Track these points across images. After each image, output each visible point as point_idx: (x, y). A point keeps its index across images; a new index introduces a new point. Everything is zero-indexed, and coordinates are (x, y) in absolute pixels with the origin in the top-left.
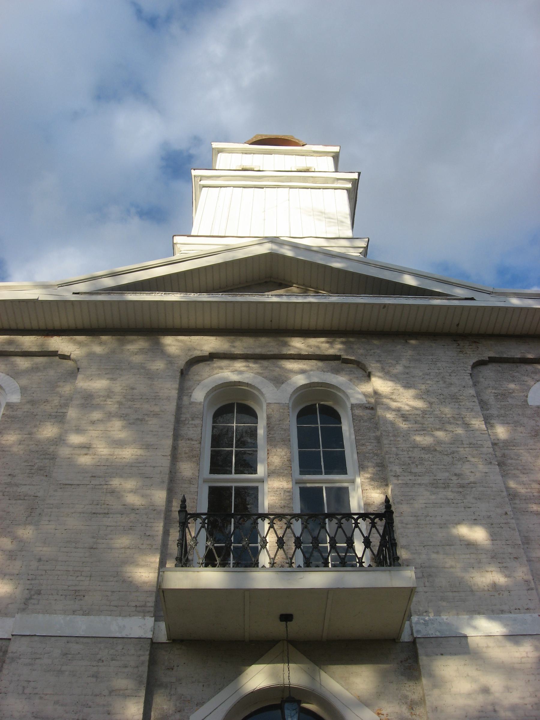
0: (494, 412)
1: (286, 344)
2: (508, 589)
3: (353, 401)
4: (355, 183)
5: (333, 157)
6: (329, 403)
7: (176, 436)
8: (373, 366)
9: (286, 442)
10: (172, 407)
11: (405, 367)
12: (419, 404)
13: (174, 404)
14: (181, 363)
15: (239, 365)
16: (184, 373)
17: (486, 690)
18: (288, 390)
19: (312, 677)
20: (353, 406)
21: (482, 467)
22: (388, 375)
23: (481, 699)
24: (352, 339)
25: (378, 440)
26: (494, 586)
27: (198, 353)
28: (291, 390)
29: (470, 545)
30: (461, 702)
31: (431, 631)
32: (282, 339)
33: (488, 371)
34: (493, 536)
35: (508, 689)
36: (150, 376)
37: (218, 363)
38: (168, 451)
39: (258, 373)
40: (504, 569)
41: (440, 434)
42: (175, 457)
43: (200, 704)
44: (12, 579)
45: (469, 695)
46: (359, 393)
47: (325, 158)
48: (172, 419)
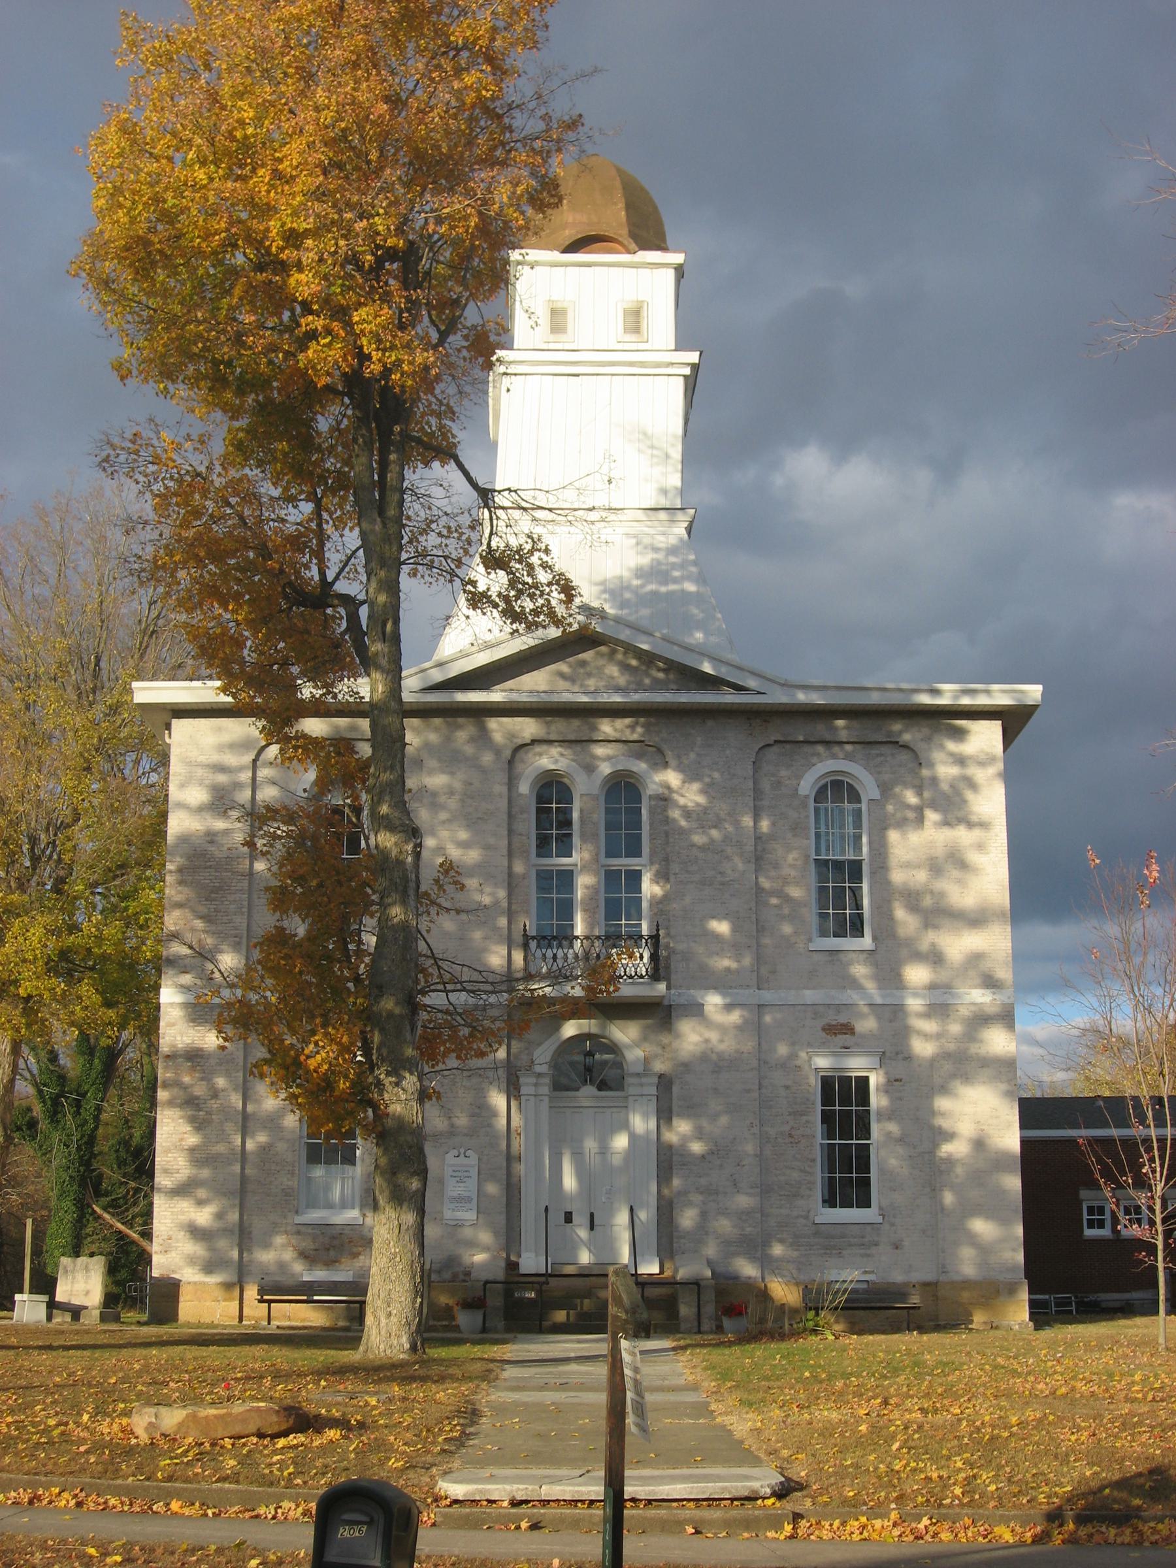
0: (765, 803)
1: (594, 728)
2: (738, 971)
3: (649, 792)
4: (695, 368)
5: (676, 269)
6: (632, 781)
7: (510, 832)
8: (669, 755)
9: (595, 835)
10: (503, 804)
11: (698, 755)
12: (701, 799)
13: (506, 801)
14: (507, 753)
15: (555, 751)
16: (511, 762)
17: (707, 1041)
18: (598, 780)
19: (603, 1027)
20: (650, 797)
21: (740, 866)
22: (680, 768)
23: (703, 1046)
24: (652, 720)
25: (667, 834)
26: (728, 970)
27: (520, 742)
28: (599, 782)
29: (717, 937)
30: (691, 1048)
31: (682, 1001)
32: (592, 720)
33: (772, 754)
34: (735, 929)
35: (722, 1041)
36: (483, 771)
37: (538, 749)
38: (505, 852)
39: (573, 760)
40: (738, 958)
41: (714, 833)
42: (510, 855)
43: (539, 1044)
44: (896, 1080)
45: (696, 1044)
46: (655, 783)
47: (663, 270)
48: (505, 817)
